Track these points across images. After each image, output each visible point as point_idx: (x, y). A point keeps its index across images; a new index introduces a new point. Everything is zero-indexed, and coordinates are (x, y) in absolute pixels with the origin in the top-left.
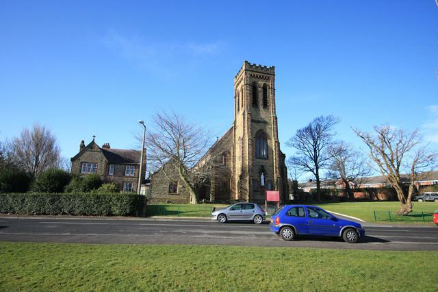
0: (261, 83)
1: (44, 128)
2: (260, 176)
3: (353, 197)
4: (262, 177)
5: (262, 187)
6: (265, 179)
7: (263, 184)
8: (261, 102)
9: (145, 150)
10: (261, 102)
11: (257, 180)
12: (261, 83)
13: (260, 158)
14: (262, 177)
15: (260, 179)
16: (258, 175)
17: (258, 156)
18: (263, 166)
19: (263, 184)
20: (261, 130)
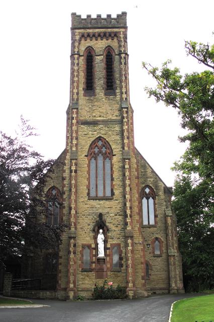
0: (100, 45)
1: (183, 140)
2: (95, 238)
3: (75, 152)
4: (101, 237)
5: (99, 260)
6: (105, 242)
7: (101, 254)
8: (99, 61)
9: (115, 155)
10: (99, 61)
11: (89, 246)
12: (100, 45)
13: (96, 198)
14: (101, 237)
15: (97, 244)
16: (92, 234)
17: (93, 194)
18: (101, 215)
19: (101, 254)
20: (100, 138)
